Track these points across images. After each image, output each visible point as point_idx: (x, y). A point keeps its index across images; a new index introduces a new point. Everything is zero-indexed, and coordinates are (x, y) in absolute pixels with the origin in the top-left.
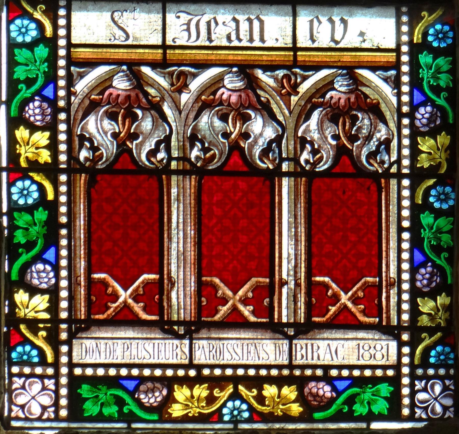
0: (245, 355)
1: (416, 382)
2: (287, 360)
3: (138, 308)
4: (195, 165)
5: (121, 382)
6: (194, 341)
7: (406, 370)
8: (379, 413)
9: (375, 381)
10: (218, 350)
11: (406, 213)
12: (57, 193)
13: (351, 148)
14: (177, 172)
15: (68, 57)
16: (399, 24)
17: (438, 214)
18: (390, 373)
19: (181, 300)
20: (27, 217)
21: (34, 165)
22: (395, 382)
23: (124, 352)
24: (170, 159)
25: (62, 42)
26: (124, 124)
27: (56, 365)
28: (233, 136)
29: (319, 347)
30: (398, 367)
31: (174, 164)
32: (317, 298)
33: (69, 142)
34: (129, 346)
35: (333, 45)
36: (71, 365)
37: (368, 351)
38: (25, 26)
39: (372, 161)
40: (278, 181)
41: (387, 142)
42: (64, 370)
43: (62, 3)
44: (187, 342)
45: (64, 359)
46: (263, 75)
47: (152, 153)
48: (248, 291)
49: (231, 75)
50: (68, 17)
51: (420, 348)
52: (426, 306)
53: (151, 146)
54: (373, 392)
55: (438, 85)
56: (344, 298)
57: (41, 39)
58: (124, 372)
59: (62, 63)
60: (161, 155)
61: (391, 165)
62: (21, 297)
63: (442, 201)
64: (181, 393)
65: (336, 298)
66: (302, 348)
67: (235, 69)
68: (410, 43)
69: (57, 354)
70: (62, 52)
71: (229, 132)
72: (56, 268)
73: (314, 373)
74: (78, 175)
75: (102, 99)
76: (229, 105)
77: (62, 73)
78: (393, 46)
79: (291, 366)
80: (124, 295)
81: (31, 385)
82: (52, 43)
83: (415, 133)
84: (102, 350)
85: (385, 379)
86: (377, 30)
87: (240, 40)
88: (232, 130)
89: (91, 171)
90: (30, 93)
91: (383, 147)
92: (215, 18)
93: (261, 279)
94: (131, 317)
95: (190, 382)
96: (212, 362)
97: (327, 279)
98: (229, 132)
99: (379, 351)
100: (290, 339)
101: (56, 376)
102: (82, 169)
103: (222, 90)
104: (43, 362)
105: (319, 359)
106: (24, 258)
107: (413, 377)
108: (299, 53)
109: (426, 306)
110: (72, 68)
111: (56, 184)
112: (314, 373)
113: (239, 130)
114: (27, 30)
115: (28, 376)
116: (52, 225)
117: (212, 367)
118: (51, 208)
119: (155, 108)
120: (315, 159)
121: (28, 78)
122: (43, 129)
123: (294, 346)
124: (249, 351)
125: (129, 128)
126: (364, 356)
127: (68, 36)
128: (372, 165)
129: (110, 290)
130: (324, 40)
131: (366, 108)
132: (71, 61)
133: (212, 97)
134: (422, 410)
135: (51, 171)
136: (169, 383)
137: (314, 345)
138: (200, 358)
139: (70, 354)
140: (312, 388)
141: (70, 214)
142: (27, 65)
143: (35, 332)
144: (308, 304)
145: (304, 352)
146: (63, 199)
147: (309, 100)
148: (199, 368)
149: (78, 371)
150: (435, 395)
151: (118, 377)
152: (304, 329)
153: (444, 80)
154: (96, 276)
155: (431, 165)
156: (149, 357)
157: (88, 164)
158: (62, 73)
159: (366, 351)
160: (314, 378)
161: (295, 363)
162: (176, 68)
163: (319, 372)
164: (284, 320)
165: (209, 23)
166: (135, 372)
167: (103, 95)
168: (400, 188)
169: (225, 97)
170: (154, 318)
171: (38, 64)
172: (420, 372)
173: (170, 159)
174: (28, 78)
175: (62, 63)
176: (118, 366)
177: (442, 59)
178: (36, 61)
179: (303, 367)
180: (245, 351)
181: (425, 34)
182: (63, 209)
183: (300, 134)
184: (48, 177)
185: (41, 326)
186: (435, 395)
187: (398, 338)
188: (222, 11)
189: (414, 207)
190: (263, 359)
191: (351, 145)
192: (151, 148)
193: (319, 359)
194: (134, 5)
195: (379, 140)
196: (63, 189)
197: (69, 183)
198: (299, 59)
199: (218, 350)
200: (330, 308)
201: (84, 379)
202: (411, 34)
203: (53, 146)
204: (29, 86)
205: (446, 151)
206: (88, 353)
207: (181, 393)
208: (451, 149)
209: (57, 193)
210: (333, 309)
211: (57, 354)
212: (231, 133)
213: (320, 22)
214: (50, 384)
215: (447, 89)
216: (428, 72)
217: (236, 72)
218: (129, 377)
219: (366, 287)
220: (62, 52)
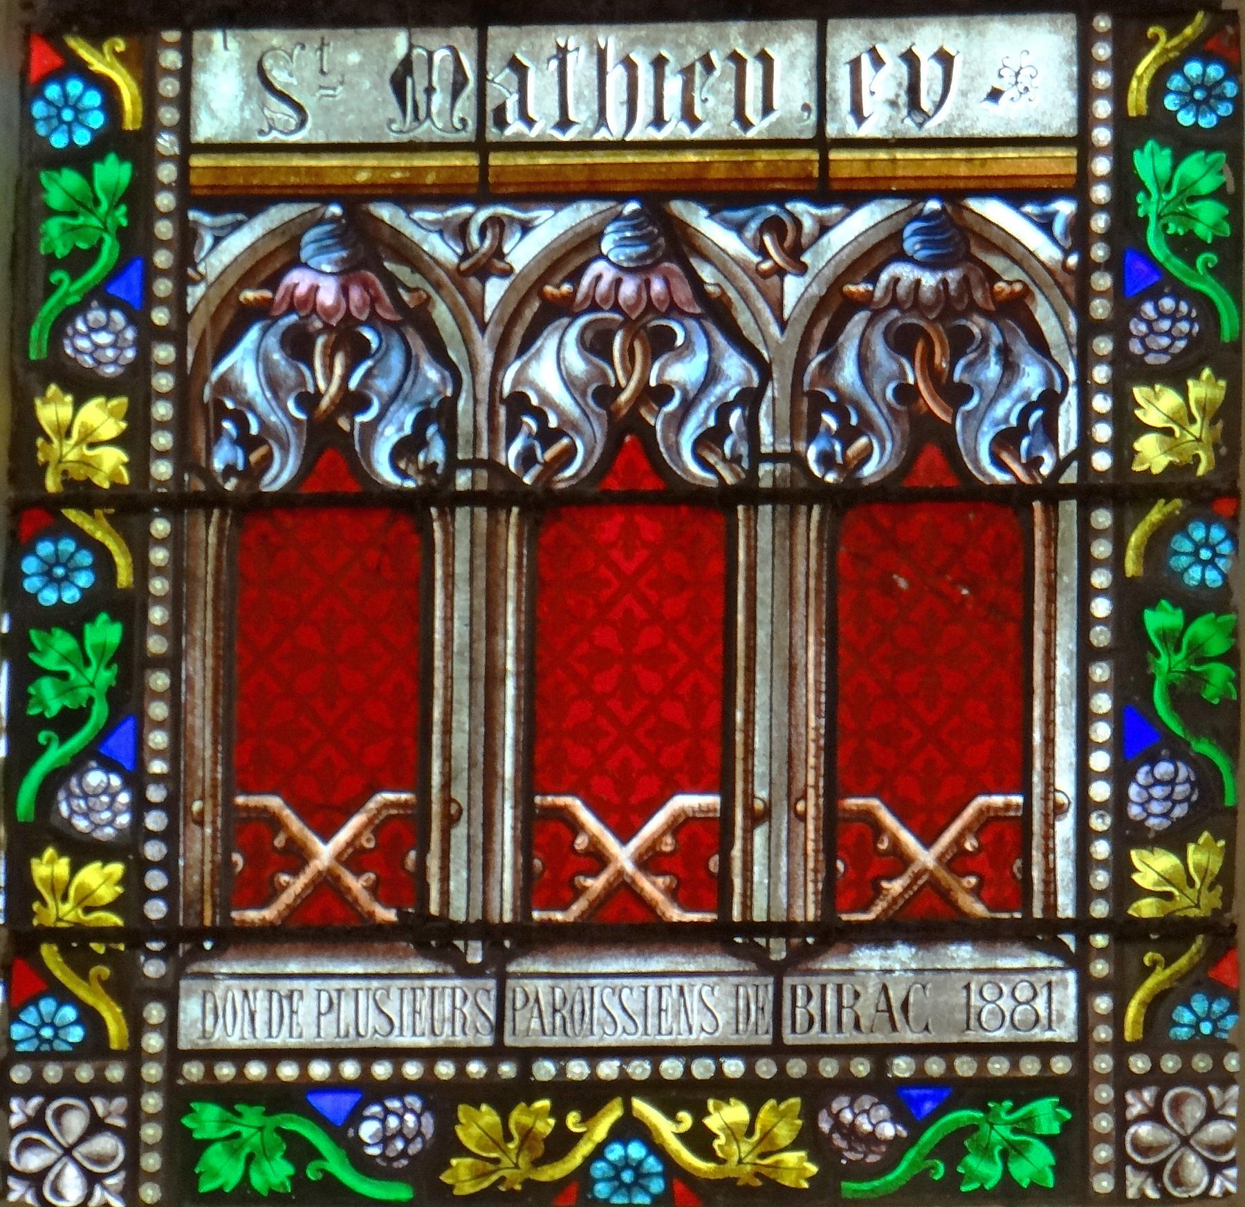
0: (652, 1021)
1: (1139, 393)
2: (767, 1032)
3: (652, 888)
4: (517, 479)
5: (311, 1099)
6: (511, 983)
7: (1103, 1063)
8: (1033, 1185)
9: (1021, 1091)
10: (577, 1008)
11: (1101, 607)
12: (143, 570)
13: (948, 419)
14: (774, 496)
15: (183, 186)
16: (1086, 64)
17: (1195, 604)
18: (1061, 1065)
19: (774, 876)
20: (63, 642)
21: (82, 493)
22: (1073, 1093)
23: (320, 1014)
24: (453, 464)
25: (166, 143)
26: (329, 369)
27: (134, 1056)
28: (624, 397)
29: (857, 995)
30: (1080, 1049)
31: (463, 480)
32: (851, 856)
33: (181, 426)
34: (335, 1001)
35: (910, 128)
36: (174, 1056)
37: (1027, 1002)
38: (71, 102)
39: (1006, 457)
40: (748, 519)
41: (1050, 400)
42: (152, 1072)
43: (150, 1193)
44: (491, 984)
45: (154, 1042)
46: (709, 222)
47: (406, 449)
48: (664, 834)
49: (617, 224)
50: (185, 76)
51: (1140, 995)
52: (1152, 867)
53: (401, 429)
54: (1016, 1122)
55: (1191, 234)
56: (325, 853)
57: (112, 139)
58: (319, 1070)
59: (165, 201)
60: (437, 452)
61: (1061, 466)
62: (53, 410)
63: (58, 583)
64: (477, 1124)
65: (297, 857)
66: (809, 996)
67: (632, 207)
68: (1120, 119)
69: (137, 1026)
70: (167, 173)
71: (613, 384)
72: (136, 780)
73: (845, 1070)
74: (803, 508)
75: (273, 299)
76: (616, 308)
77: (164, 229)
78: (1072, 131)
79: (778, 1050)
80: (623, 855)
81: (59, 1114)
82: (135, 146)
83: (1130, 371)
84: (240, 1010)
85: (1043, 1086)
86: (1018, 77)
87: (530, 122)
88: (623, 382)
89: (249, 507)
90: (77, 292)
91: (1037, 414)
92: (873, 51)
93: (998, 800)
94: (639, 917)
95: (504, 1097)
96: (558, 1041)
97: (274, 802)
98: (613, 384)
99: (1029, 999)
100: (778, 971)
101: (134, 1087)
102: (213, 499)
103: (598, 267)
104: (95, 1045)
105: (857, 1026)
106: (55, 755)
107: (1124, 1081)
108: (833, 155)
109: (1152, 867)
110: (193, 215)
111: (139, 546)
112: (845, 1070)
113: (640, 381)
114: (66, 578)
115: (51, 1093)
116: (130, 660)
117: (561, 1054)
118: (129, 609)
119: (717, 312)
120: (850, 452)
121: (75, 250)
122: (108, 388)
123: (787, 995)
124: (664, 1007)
125: (346, 378)
126: (1000, 1018)
127: (184, 128)
128: (1003, 467)
129: (581, 842)
130: (716, 119)
131: (992, 307)
132: (188, 196)
133: (566, 288)
134: (1144, 1174)
135: (129, 506)
136: (443, 1100)
137: (844, 987)
138: (527, 1029)
139: (171, 1027)
140: (840, 1111)
141: (176, 629)
142: (73, 214)
143: (81, 962)
144: (526, 876)
145: (814, 1006)
146: (158, 586)
147: (836, 285)
148: (526, 1056)
149: (193, 1071)
150: (1182, 1125)
151: (306, 1086)
152: (507, 943)
153: (1208, 218)
154: (853, 803)
155: (1171, 464)
156: (388, 1028)
157: (230, 485)
158: (164, 229)
159: (1020, 1003)
160: (848, 1085)
161: (789, 1039)
162: (467, 209)
163: (861, 1068)
164: (759, 915)
165: (855, 64)
166: (350, 1070)
167: (274, 291)
168: (1087, 534)
169: (603, 286)
170: (709, 917)
171: (104, 206)
172: (1139, 1064)
173: (757, 456)
174: (75, 250)
175: (165, 201)
176: (303, 1056)
177: (1199, 160)
178: (97, 202)
179: (813, 1052)
180: (407, 1009)
181: (1157, 89)
182: (157, 615)
183: (507, 389)
184: (116, 523)
185: (99, 948)
186: (1182, 1125)
187: (1079, 962)
188: (850, 28)
189: (1122, 590)
190: (376, 1031)
191: (945, 411)
192: (402, 434)
193: (857, 1026)
194: (324, 32)
195: (1025, 395)
196: (159, 556)
197: (176, 542)
198: (835, 172)
199: (577, 1008)
200: (284, 878)
201: (212, 1091)
202: (1119, 93)
203: (134, 439)
204: (75, 275)
205: (1213, 422)
206: (221, 1020)
207: (477, 1124)
208: (1225, 415)
209: (143, 570)
210: (896, 886)
211: (137, 1026)
212: (619, 389)
213: (878, 62)
214: (113, 1109)
215: (1218, 244)
216: (1160, 198)
217: (635, 214)
218: (335, 1085)
219: (988, 822)
220: (167, 173)
